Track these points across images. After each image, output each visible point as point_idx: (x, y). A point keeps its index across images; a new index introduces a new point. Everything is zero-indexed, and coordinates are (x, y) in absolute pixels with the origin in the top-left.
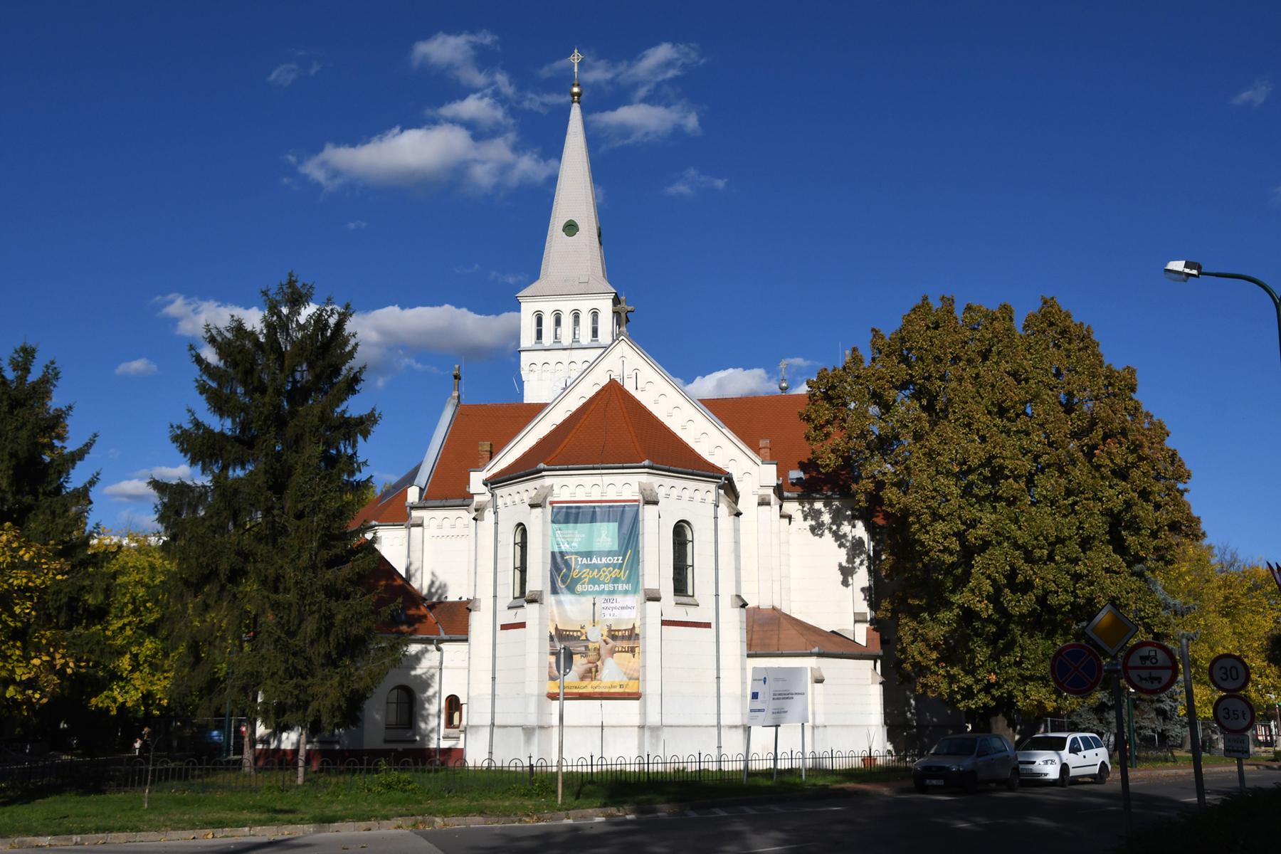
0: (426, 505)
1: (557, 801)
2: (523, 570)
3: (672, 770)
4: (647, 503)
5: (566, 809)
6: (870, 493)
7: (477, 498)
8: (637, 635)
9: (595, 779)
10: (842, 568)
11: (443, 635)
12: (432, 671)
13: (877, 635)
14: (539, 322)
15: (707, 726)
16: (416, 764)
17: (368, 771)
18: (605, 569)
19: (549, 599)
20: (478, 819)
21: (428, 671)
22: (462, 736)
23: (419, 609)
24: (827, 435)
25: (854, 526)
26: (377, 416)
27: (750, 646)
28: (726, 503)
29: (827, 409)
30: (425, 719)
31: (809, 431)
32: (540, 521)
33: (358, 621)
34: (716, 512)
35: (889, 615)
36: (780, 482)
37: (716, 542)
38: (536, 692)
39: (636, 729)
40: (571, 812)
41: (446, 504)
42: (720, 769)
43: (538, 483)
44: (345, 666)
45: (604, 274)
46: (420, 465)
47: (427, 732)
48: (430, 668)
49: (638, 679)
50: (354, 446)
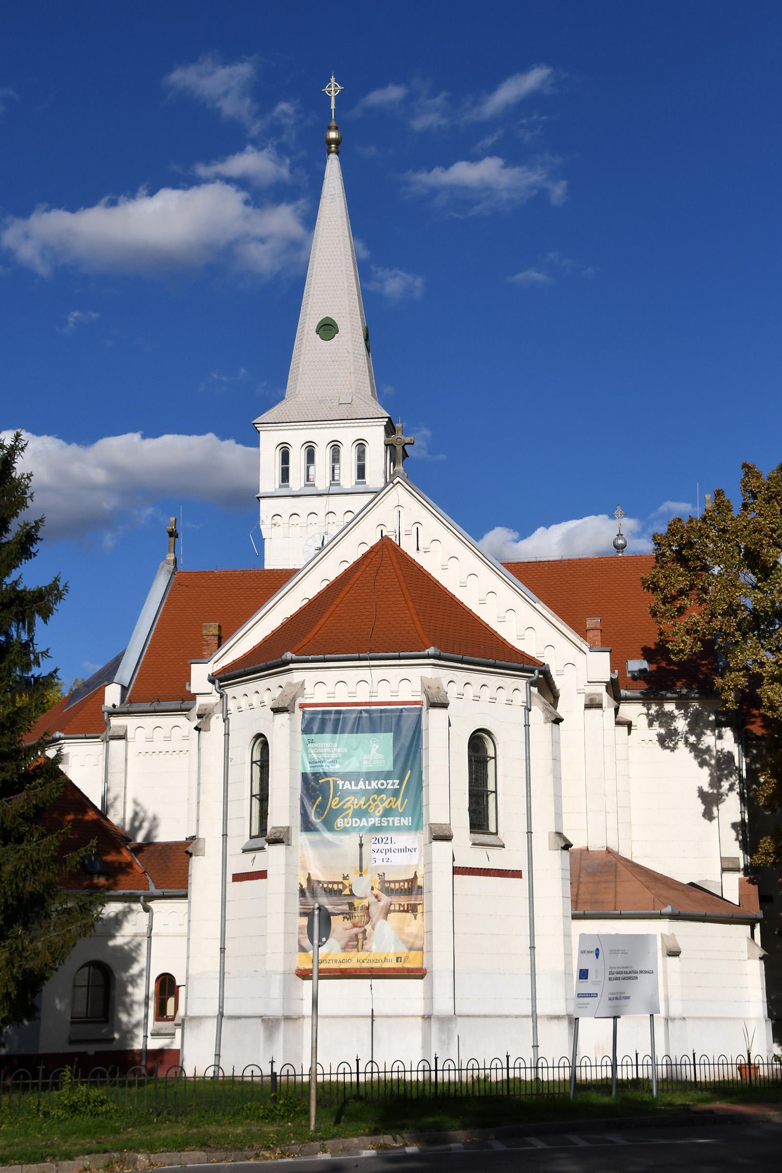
0: (131, 709)
1: (309, 1126)
2: (263, 798)
3: (470, 1079)
4: (433, 705)
5: (322, 1139)
6: (742, 691)
7: (200, 700)
8: (420, 887)
9: (362, 1093)
10: (702, 794)
11: (153, 890)
12: (138, 939)
13: (754, 890)
14: (285, 458)
15: (516, 1017)
16: (113, 1074)
17: (45, 1087)
18: (375, 796)
19: (300, 838)
20: (199, 1154)
21: (132, 940)
22: (178, 1032)
23: (119, 852)
24: (681, 611)
25: (720, 737)
26: (61, 588)
27: (575, 903)
28: (541, 705)
29: (681, 575)
30: (129, 1012)
32: (286, 731)
33: (34, 873)
34: (527, 718)
35: (771, 860)
36: (614, 677)
37: (528, 759)
38: (281, 969)
39: (420, 1020)
40: (329, 1143)
41: (158, 708)
42: (537, 1078)
43: (283, 679)
44: (17, 937)
45: (372, 392)
46: (122, 654)
47: (130, 1026)
48: (135, 936)
49: (422, 950)
50: (30, 630)
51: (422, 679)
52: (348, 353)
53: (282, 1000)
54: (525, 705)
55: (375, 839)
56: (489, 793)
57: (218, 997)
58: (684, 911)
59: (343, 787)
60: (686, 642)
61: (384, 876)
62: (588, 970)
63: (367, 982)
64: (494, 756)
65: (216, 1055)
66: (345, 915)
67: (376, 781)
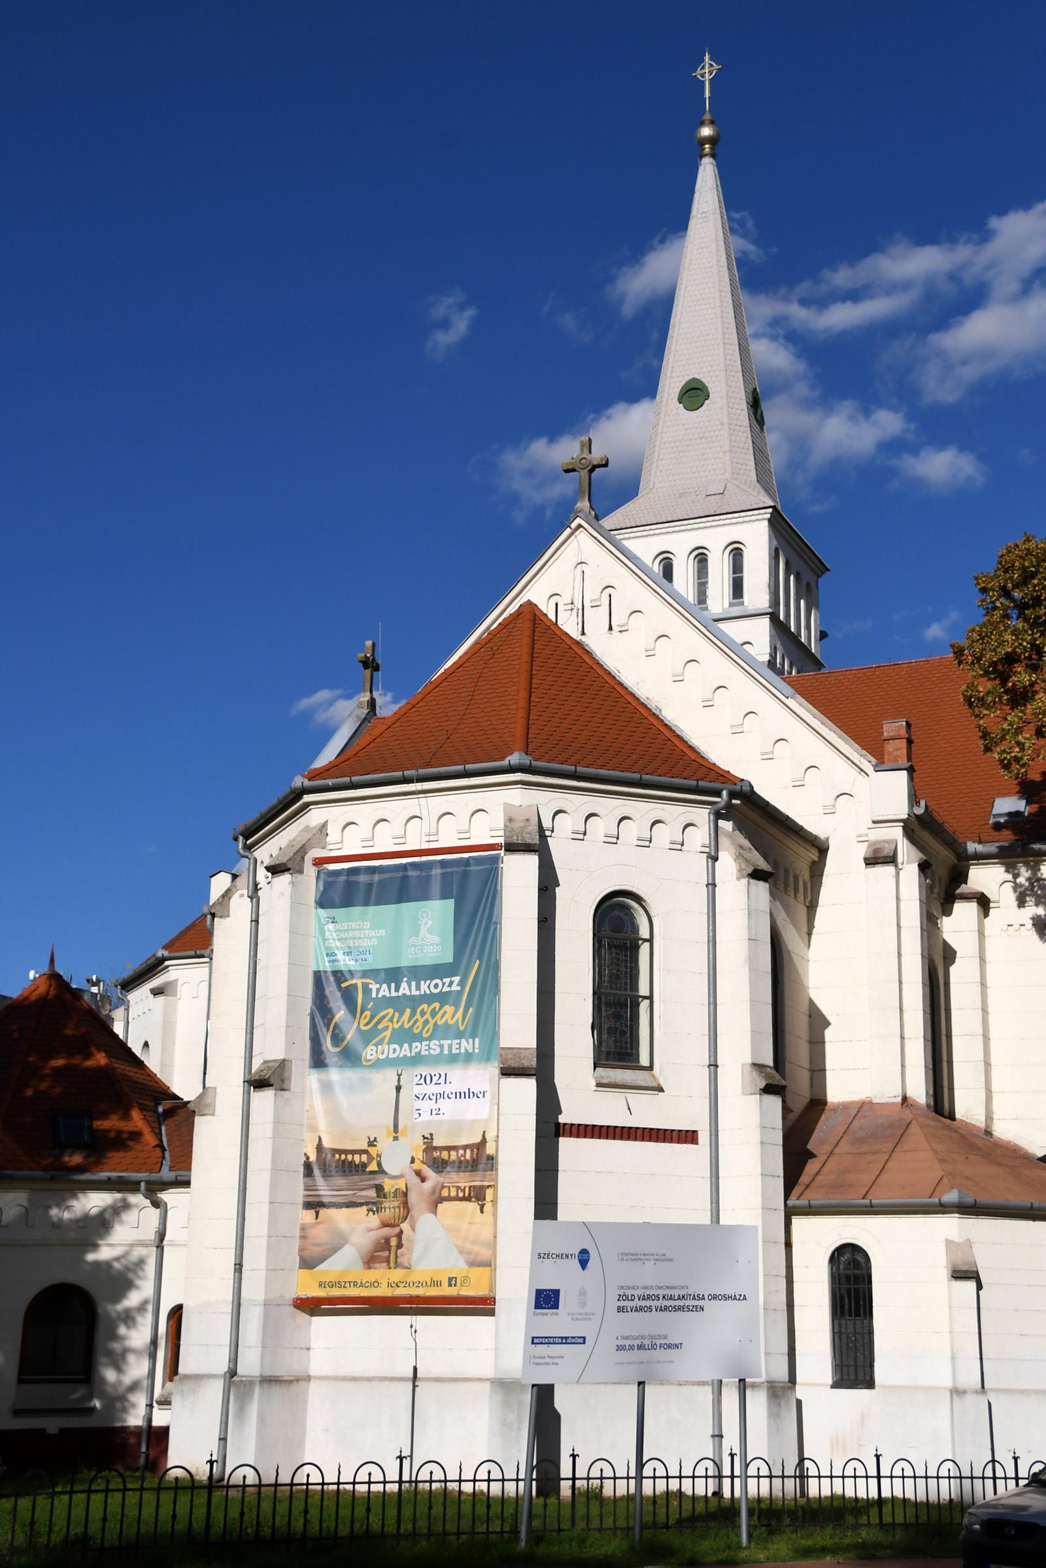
8: (491, 1158)
12: (138, 1252)
19: (306, 1080)
21: (127, 1254)
30: (118, 1361)
31: (972, 686)
39: (488, 1385)
47: (122, 1390)
51: (507, 806)
52: (722, 424)
53: (260, 1349)
54: (707, 850)
55: (419, 1076)
56: (640, 999)
57: (229, 1343)
58: (983, 1199)
59: (377, 994)
60: (1023, 744)
61: (432, 1139)
62: (559, 1290)
63: (406, 1320)
64: (648, 937)
65: (220, 1439)
66: (370, 1206)
67: (428, 982)
